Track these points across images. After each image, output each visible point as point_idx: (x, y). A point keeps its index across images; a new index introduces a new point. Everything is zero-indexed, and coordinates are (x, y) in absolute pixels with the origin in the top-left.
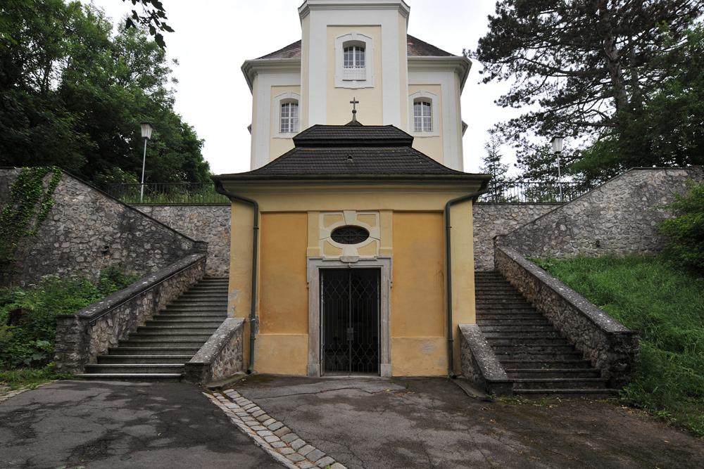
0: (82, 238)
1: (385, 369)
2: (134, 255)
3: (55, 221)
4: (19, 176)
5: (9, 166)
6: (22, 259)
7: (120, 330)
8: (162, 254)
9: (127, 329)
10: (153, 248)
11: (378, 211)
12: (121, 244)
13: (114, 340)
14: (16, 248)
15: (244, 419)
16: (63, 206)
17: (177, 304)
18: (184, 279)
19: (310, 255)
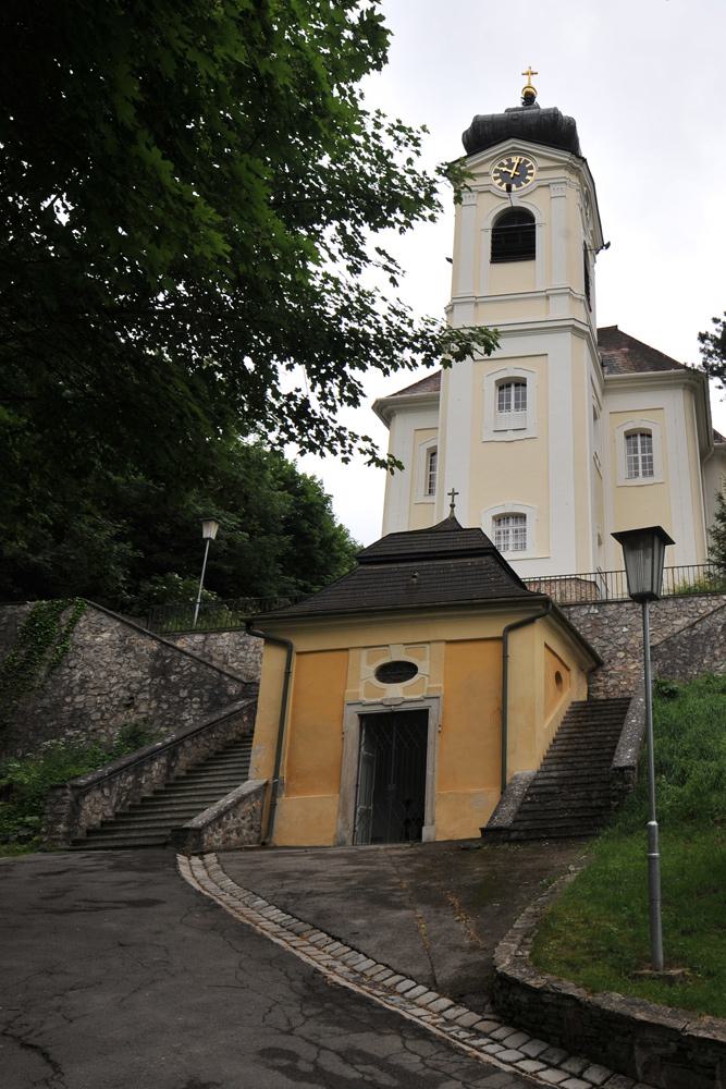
0: (102, 688)
1: (428, 833)
2: (165, 706)
3: (71, 668)
4: (32, 613)
5: (19, 600)
6: (22, 720)
7: (119, 800)
8: (201, 703)
9: (127, 800)
10: (190, 696)
11: (428, 642)
12: (150, 691)
13: (109, 812)
14: (17, 707)
16: (82, 648)
17: (199, 768)
18: (218, 735)
19: (348, 699)
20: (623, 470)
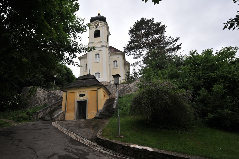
0: (41, 98)
1: (87, 118)
13: (42, 116)
15: (96, 148)
20: (113, 66)
